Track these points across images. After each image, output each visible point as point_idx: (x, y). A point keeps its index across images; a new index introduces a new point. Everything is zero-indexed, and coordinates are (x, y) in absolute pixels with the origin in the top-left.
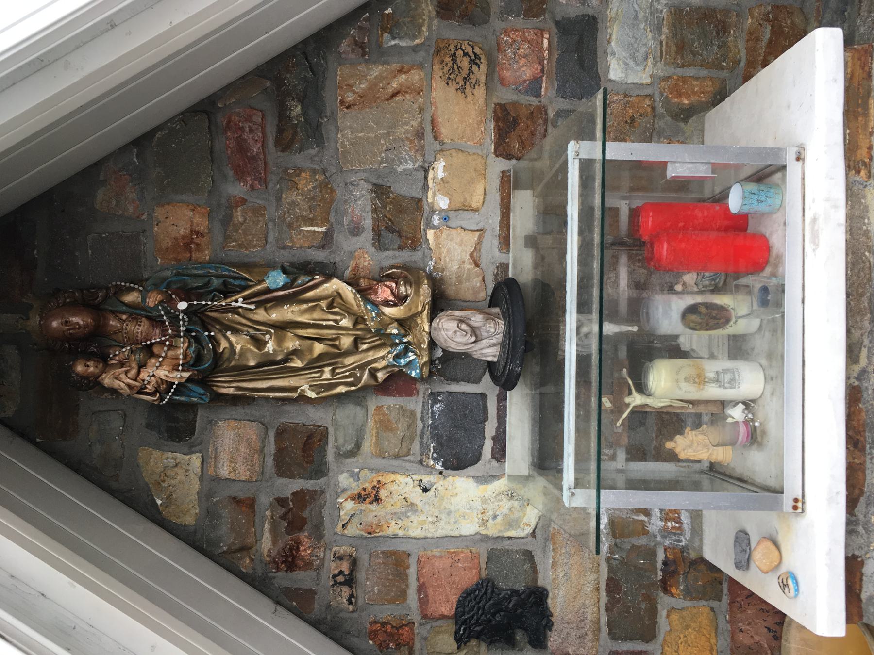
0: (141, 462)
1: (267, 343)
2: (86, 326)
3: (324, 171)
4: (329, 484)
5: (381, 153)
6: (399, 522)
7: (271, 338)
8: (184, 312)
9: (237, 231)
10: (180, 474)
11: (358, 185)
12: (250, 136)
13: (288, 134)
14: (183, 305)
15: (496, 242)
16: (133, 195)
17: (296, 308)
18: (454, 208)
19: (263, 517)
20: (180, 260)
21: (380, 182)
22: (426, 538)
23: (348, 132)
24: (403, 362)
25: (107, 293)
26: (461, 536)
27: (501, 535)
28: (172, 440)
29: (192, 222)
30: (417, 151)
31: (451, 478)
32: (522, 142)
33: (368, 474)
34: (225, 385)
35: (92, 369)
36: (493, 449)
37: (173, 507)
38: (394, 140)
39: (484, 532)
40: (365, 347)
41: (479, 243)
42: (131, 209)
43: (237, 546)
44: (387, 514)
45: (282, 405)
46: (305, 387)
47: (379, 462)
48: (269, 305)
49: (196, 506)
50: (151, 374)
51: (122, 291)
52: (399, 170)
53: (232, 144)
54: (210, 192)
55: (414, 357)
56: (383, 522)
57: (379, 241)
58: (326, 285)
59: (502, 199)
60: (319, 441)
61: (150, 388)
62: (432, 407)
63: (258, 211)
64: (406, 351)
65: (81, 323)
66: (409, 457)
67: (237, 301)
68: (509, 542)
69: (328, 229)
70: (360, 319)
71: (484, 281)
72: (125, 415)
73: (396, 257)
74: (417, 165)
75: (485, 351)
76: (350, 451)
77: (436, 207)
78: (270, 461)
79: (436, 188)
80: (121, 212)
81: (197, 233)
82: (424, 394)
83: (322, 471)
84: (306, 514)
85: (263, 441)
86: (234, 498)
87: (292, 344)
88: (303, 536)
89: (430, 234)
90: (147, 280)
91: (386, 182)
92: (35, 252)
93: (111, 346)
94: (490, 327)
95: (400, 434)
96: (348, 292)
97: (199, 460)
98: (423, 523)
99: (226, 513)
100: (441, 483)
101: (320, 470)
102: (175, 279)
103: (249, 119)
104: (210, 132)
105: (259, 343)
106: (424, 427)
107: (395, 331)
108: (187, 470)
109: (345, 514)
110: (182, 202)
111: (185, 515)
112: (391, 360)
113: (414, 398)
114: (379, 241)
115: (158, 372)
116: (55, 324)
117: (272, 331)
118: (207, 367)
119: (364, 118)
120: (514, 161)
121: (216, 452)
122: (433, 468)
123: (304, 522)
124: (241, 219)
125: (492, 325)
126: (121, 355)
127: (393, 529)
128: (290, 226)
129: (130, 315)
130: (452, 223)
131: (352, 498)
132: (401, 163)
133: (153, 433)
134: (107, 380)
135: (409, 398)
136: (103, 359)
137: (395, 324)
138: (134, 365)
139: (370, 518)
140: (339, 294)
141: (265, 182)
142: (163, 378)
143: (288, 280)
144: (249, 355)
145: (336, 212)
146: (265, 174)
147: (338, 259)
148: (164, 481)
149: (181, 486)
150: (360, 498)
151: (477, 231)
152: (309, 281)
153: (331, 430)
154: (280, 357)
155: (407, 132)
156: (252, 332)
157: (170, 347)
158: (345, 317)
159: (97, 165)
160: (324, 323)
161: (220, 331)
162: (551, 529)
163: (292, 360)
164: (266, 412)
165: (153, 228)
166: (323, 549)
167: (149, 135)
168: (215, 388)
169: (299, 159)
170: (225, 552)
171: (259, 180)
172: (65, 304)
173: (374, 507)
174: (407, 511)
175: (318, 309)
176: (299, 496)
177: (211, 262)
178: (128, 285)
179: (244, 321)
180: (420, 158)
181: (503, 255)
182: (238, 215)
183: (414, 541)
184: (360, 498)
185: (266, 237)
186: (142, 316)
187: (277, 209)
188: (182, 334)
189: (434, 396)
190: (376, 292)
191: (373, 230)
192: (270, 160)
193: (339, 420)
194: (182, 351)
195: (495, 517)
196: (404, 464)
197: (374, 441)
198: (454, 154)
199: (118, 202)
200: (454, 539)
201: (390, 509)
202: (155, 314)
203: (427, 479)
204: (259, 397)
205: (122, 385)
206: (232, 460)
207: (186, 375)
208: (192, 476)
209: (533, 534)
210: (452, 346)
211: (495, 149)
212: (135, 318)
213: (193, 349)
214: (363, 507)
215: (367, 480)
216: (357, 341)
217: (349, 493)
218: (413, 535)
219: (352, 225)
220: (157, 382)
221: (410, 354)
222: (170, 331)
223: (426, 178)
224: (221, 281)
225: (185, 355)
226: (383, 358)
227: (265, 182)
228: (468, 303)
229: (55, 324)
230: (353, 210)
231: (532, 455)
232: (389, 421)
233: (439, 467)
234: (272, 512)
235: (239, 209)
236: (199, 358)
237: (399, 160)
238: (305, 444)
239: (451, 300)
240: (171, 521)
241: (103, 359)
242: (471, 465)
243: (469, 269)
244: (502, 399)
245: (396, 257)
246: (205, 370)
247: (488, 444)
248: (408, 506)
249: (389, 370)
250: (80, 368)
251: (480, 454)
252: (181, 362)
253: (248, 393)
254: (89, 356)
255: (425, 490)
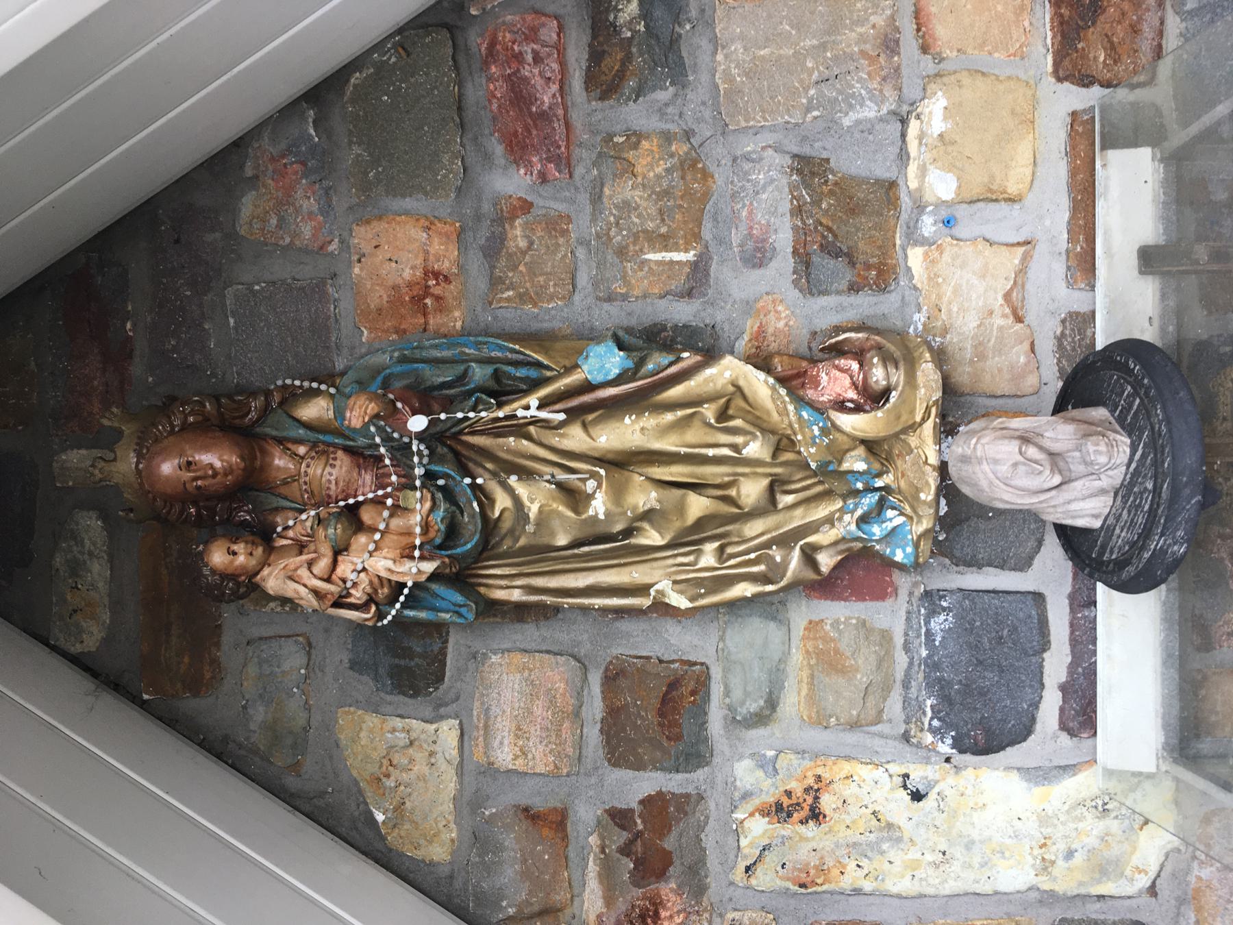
0: (343, 737)
1: (591, 497)
2: (228, 471)
3: (688, 135)
4: (713, 784)
5: (806, 90)
6: (864, 862)
7: (599, 486)
8: (421, 436)
9: (515, 268)
10: (417, 761)
11: (761, 159)
12: (536, 71)
13: (612, 62)
14: (418, 423)
15: (1060, 267)
16: (310, 204)
17: (650, 421)
18: (968, 196)
19: (584, 849)
20: (405, 331)
21: (806, 150)
22: (922, 896)
23: (737, 47)
24: (877, 530)
25: (267, 404)
26: (996, 893)
27: (1083, 891)
28: (405, 694)
29: (427, 252)
30: (884, 79)
31: (970, 770)
32: (1113, 47)
33: (795, 762)
34: (503, 583)
35: (241, 559)
36: (1062, 710)
37: (407, 826)
38: (836, 58)
39: (1046, 887)
40: (789, 499)
41: (1022, 271)
42: (307, 231)
43: (536, 908)
44: (837, 845)
45: (614, 620)
46: (665, 585)
47: (817, 738)
48: (590, 417)
49: (453, 826)
50: (360, 567)
51: (292, 397)
52: (847, 122)
53: (500, 89)
54: (459, 190)
55: (902, 519)
56: (830, 862)
57: (808, 275)
58: (709, 372)
59: (1073, 173)
60: (693, 693)
61: (358, 596)
62: (927, 623)
63: (556, 225)
64: (881, 505)
65: (218, 464)
66: (879, 728)
67: (527, 408)
68: (1098, 905)
69: (700, 256)
70: (785, 441)
71: (1033, 351)
72: (310, 645)
73: (843, 309)
74: (884, 111)
75: (1075, 506)
76: (756, 715)
77: (929, 197)
78: (593, 734)
79: (928, 157)
80: (288, 240)
81: (436, 275)
82: (911, 594)
83: (699, 756)
84: (669, 843)
85: (579, 695)
86: (526, 810)
87: (643, 497)
88: (667, 890)
89: (915, 258)
90: (343, 374)
91: (816, 150)
92: (129, 326)
93: (277, 510)
94: (1097, 450)
95: (862, 679)
96: (759, 385)
97: (455, 733)
98: (914, 865)
99: (511, 840)
100: (951, 780)
101: (695, 755)
102: (398, 369)
103: (532, 35)
104: (456, 67)
105: (574, 497)
106: (911, 664)
107: (861, 466)
108: (432, 754)
109: (751, 845)
110: (407, 213)
111: (430, 842)
112: (853, 527)
113: (889, 602)
114: (808, 275)
115: (374, 562)
116: (167, 468)
117: (602, 472)
118: (467, 552)
119: (770, 16)
120: (1096, 90)
121: (487, 718)
122: (931, 749)
123: (666, 859)
124: (523, 244)
125: (1103, 448)
126: (299, 528)
127: (852, 877)
128: (621, 252)
129: (314, 445)
130: (961, 230)
131: (764, 812)
132: (851, 107)
133: (365, 678)
134: (273, 581)
135: (878, 604)
136: (264, 535)
137: (861, 451)
138: (326, 550)
139: (803, 854)
140: (739, 388)
141: (569, 165)
142: (383, 574)
143: (630, 364)
144: (556, 524)
145: (715, 220)
146: (567, 147)
147: (720, 317)
148: (388, 776)
149: (421, 784)
150: (780, 811)
151: (1018, 244)
152: (671, 364)
153: (716, 673)
154: (618, 527)
155: (862, 39)
156: (562, 476)
157: (396, 509)
158: (755, 437)
159: (239, 145)
160: (711, 452)
161: (494, 475)
162: (1192, 879)
163: (638, 529)
164: (580, 634)
165: (350, 265)
166: (706, 915)
167: (335, 81)
168: (482, 590)
169: (634, 114)
170: (510, 918)
171: (556, 159)
172: (185, 427)
173: (811, 829)
174: (880, 840)
175: (697, 423)
176: (656, 804)
177: (465, 332)
178: (306, 384)
179: (542, 453)
180: (889, 92)
181: (1077, 294)
182: (517, 235)
183: (896, 902)
184: (780, 811)
185: (573, 278)
186: (335, 446)
187: (594, 220)
188: (418, 483)
189: (931, 599)
190: (816, 383)
191: (795, 252)
192: (576, 118)
193: (733, 650)
194: (418, 518)
195: (1070, 854)
196: (869, 741)
197: (804, 692)
198: (966, 80)
199: (281, 220)
200: (981, 900)
201: (843, 835)
202: (362, 441)
203: (919, 774)
204: (572, 607)
205: (303, 591)
206: (519, 732)
207: (429, 567)
208: (443, 766)
209: (1152, 890)
210: (1006, 497)
211: (1057, 65)
212: (324, 452)
213: (440, 513)
214: (787, 830)
215: (793, 776)
216: (776, 486)
217: (756, 802)
218: (894, 890)
219: (750, 245)
220: (371, 583)
221: (890, 513)
222: (394, 478)
223: (903, 135)
224: (489, 370)
225: (426, 527)
226: (830, 521)
227: (566, 163)
228: (1001, 401)
229: (167, 468)
230: (750, 213)
231: (1166, 726)
232: (837, 651)
233: (945, 748)
234: (602, 838)
235: (518, 222)
236: (453, 532)
237: (845, 100)
238: (665, 700)
239: (962, 394)
240: (402, 855)
241: (264, 535)
242: (1012, 743)
243: (1001, 328)
244: (1083, 602)
245: (843, 309)
246: (464, 556)
247: (1051, 701)
248: (881, 829)
249: (842, 547)
250: (218, 557)
251: (1033, 720)
252: (418, 542)
253: (549, 600)
254: (234, 531)
255: (917, 796)
